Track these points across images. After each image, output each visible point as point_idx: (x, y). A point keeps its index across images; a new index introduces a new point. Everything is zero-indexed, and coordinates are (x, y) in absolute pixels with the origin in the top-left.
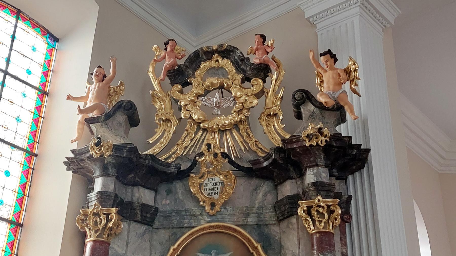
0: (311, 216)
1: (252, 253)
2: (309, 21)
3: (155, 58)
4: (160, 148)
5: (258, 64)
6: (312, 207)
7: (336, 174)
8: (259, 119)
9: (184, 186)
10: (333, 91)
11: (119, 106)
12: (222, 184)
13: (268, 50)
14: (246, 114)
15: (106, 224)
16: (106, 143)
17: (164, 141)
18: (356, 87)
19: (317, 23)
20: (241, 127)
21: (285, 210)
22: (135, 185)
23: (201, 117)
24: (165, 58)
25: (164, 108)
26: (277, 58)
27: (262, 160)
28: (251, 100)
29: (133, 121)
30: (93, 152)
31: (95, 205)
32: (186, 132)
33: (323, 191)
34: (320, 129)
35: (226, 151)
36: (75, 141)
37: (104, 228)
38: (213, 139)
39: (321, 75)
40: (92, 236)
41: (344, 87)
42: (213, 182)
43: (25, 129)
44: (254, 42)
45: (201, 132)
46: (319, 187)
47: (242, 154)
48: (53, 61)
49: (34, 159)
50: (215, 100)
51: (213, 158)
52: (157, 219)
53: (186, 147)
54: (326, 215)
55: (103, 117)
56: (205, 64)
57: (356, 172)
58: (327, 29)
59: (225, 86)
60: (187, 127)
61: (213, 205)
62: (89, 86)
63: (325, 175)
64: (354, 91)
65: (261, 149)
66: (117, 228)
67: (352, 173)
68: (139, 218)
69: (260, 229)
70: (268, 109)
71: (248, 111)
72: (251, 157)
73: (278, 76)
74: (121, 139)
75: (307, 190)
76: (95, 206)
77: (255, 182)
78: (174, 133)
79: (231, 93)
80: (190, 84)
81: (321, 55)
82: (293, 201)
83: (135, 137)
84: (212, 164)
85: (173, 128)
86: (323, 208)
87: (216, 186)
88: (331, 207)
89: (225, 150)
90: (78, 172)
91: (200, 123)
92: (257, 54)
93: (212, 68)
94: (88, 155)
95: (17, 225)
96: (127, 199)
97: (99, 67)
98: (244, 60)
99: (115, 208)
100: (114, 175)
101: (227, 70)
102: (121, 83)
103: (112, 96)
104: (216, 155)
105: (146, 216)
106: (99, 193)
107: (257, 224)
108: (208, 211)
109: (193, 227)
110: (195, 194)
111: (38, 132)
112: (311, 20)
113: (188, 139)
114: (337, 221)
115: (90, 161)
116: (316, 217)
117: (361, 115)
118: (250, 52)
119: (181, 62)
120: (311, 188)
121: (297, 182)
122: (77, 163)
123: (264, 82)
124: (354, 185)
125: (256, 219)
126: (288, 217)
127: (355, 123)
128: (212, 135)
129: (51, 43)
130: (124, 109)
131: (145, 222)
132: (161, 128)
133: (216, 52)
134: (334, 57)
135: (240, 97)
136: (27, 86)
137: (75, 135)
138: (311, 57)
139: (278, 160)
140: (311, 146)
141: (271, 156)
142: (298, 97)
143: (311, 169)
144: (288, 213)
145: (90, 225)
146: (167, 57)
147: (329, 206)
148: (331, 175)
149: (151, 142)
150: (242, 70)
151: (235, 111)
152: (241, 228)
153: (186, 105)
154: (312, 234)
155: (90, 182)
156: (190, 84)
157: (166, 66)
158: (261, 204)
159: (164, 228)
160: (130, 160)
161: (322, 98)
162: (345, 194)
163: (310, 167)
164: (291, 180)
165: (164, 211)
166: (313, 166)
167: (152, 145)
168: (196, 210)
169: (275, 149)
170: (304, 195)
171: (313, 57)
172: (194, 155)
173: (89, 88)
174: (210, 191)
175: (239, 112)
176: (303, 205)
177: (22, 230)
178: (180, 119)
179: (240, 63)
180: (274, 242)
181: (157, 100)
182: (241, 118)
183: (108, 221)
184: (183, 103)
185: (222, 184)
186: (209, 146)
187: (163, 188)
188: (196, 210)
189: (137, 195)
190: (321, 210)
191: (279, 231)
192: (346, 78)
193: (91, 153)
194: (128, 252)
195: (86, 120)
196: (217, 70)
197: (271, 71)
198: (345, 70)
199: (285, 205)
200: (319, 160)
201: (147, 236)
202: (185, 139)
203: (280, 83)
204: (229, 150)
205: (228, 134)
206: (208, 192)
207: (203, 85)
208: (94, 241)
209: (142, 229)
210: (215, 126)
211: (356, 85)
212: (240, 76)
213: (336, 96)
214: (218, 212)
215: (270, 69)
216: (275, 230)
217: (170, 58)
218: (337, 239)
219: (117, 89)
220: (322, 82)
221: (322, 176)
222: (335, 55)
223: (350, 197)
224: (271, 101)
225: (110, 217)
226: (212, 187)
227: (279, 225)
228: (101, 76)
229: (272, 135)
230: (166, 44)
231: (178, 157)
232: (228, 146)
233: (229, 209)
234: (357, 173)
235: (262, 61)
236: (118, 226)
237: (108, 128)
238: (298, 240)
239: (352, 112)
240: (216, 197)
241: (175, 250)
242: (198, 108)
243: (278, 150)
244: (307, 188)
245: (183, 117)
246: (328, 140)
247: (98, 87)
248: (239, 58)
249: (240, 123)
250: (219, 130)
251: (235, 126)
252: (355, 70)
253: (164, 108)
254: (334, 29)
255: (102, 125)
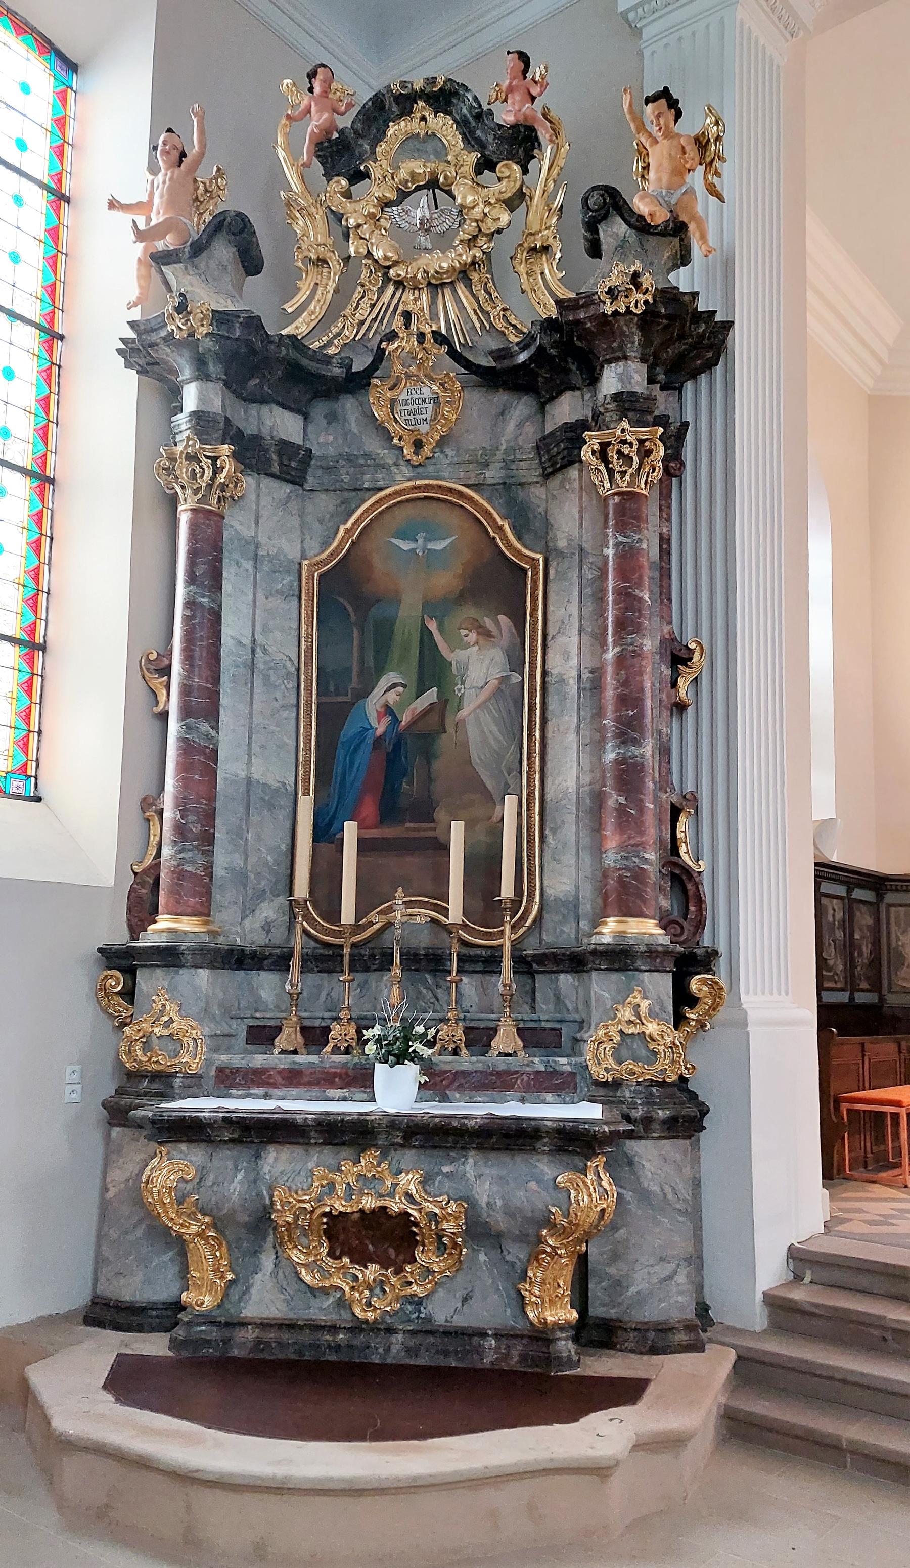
0: (607, 463)
1: (494, 538)
2: (627, 21)
3: (289, 112)
4: (308, 324)
5: (512, 127)
6: (609, 443)
7: (661, 377)
8: (511, 258)
9: (361, 405)
10: (669, 188)
11: (219, 225)
12: (436, 400)
13: (535, 91)
14: (485, 246)
15: (213, 479)
16: (198, 307)
17: (317, 309)
18: (716, 180)
19: (644, 26)
20: (475, 277)
21: (558, 453)
22: (263, 401)
23: (390, 254)
24: (309, 112)
25: (312, 233)
26: (553, 114)
27: (516, 348)
28: (495, 213)
29: (251, 263)
30: (174, 327)
31: (188, 438)
32: (359, 288)
33: (634, 410)
34: (635, 276)
35: (443, 331)
36: (135, 305)
37: (210, 486)
38: (415, 300)
39: (645, 152)
40: (189, 500)
41: (693, 180)
42: (417, 396)
43: (32, 277)
44: (504, 70)
45: (391, 289)
46: (628, 404)
47: (476, 338)
48: (72, 121)
49: (58, 345)
50: (419, 214)
51: (416, 343)
52: (310, 471)
53: (362, 323)
54: (635, 458)
55: (186, 250)
56: (396, 127)
57: (700, 373)
58: (665, 41)
59: (442, 180)
60: (362, 276)
61: (418, 445)
62: (152, 177)
63: (639, 379)
64: (713, 190)
65: (514, 326)
66: (236, 486)
67: (694, 375)
68: (276, 468)
69: (508, 490)
70: (531, 234)
71: (490, 241)
72: (495, 344)
73: (555, 157)
74: (229, 301)
75: (601, 410)
76: (188, 442)
77: (502, 397)
78: (336, 291)
79: (454, 197)
80: (366, 175)
81: (648, 101)
82: (573, 434)
83: (254, 296)
84: (415, 358)
85: (334, 280)
86: (631, 445)
87: (424, 406)
88: (647, 444)
89: (440, 328)
90: (147, 372)
91: (389, 268)
92: (509, 101)
93: (413, 137)
94: (163, 333)
95: (32, 646)
96: (250, 429)
97: (170, 130)
98: (481, 115)
99: (226, 446)
100: (220, 379)
101: (445, 141)
102: (219, 169)
103: (201, 202)
104: (421, 336)
105: (290, 466)
106: (194, 414)
107: (505, 483)
108: (409, 458)
109: (381, 489)
110: (383, 422)
111: (59, 286)
112: (631, 16)
113: (365, 304)
114: (655, 474)
115: (168, 346)
116: (616, 464)
117: (722, 245)
118: (495, 97)
119: (345, 122)
120: (608, 406)
121: (583, 396)
122: (144, 352)
123: (525, 171)
124: (695, 400)
125: (503, 473)
126: (563, 467)
127: (708, 262)
128: (413, 294)
129: (62, 74)
130: (230, 232)
131: (288, 477)
132: (309, 278)
133: (420, 98)
134: (673, 104)
135: (473, 208)
136: (23, 180)
137: (134, 293)
138: (626, 107)
139: (548, 347)
140: (616, 313)
141: (533, 338)
142: (595, 204)
143: (613, 365)
144: (562, 459)
145: (183, 478)
146: (313, 109)
147: (641, 442)
148: (651, 380)
149: (290, 310)
150: (479, 141)
151: (461, 241)
152: (472, 490)
153: (359, 226)
154: (606, 499)
155: (174, 393)
156: (366, 175)
157: (313, 130)
158: (512, 444)
159: (327, 490)
160: (249, 344)
161: (646, 205)
162: (676, 419)
163: (609, 362)
164: (571, 392)
165: (324, 458)
166: (617, 359)
167: (293, 317)
168: (386, 455)
169: (542, 323)
170: (596, 421)
171: (630, 105)
172: (378, 337)
173: (153, 181)
174: (412, 417)
175: (471, 242)
176: (592, 440)
177: (53, 490)
178: (347, 259)
179: (474, 124)
180: (535, 517)
181: (298, 215)
182: (475, 257)
183: (216, 471)
184: (352, 222)
185: (436, 400)
186: (407, 315)
187: (319, 410)
188: (386, 455)
189: (269, 423)
190: (626, 450)
191: (544, 497)
192: (697, 159)
193: (169, 328)
194: (260, 535)
195: (152, 256)
196: (424, 141)
197: (540, 144)
198: (697, 140)
199: (557, 445)
200: (629, 345)
201: (294, 506)
202: (358, 304)
203: (558, 175)
204: (449, 328)
205: (448, 291)
206: (407, 417)
207: (393, 178)
208: (194, 510)
209: (283, 491)
210: (419, 276)
211: (717, 174)
212: (472, 158)
213: (673, 201)
214: (427, 459)
215: (537, 138)
216: (537, 495)
217: (320, 111)
218: (652, 510)
219: (211, 186)
220: (646, 168)
221: (633, 381)
222: (677, 101)
223: (686, 424)
224: (539, 218)
225: (218, 462)
226: (416, 407)
227: (544, 484)
228: (176, 154)
229: (538, 294)
230: (312, 75)
231: (345, 344)
232: (447, 321)
233: (449, 451)
234: (703, 375)
235: (521, 118)
236: (236, 484)
237: (200, 275)
238: (581, 512)
239: (703, 237)
240: (424, 428)
241: (347, 531)
242: (384, 232)
243: (549, 325)
244: (603, 405)
245: (353, 254)
246: (651, 301)
247: (171, 179)
248: (470, 113)
249: (472, 268)
250: (429, 284)
251: (461, 275)
252: (718, 138)
253: (312, 233)
254: (680, 39)
255: (186, 268)
